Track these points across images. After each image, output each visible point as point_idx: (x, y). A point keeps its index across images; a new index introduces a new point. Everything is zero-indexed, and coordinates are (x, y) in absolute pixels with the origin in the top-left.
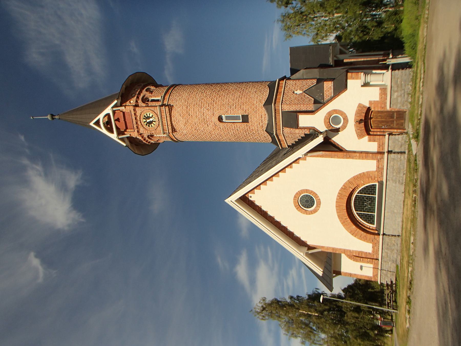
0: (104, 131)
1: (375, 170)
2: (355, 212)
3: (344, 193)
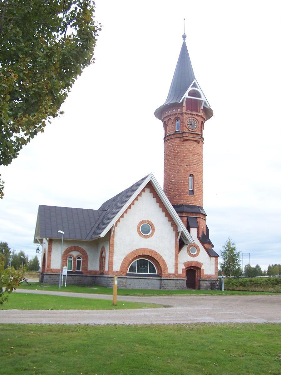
0: (190, 89)
1: (169, 273)
2: (137, 260)
3: (153, 254)
